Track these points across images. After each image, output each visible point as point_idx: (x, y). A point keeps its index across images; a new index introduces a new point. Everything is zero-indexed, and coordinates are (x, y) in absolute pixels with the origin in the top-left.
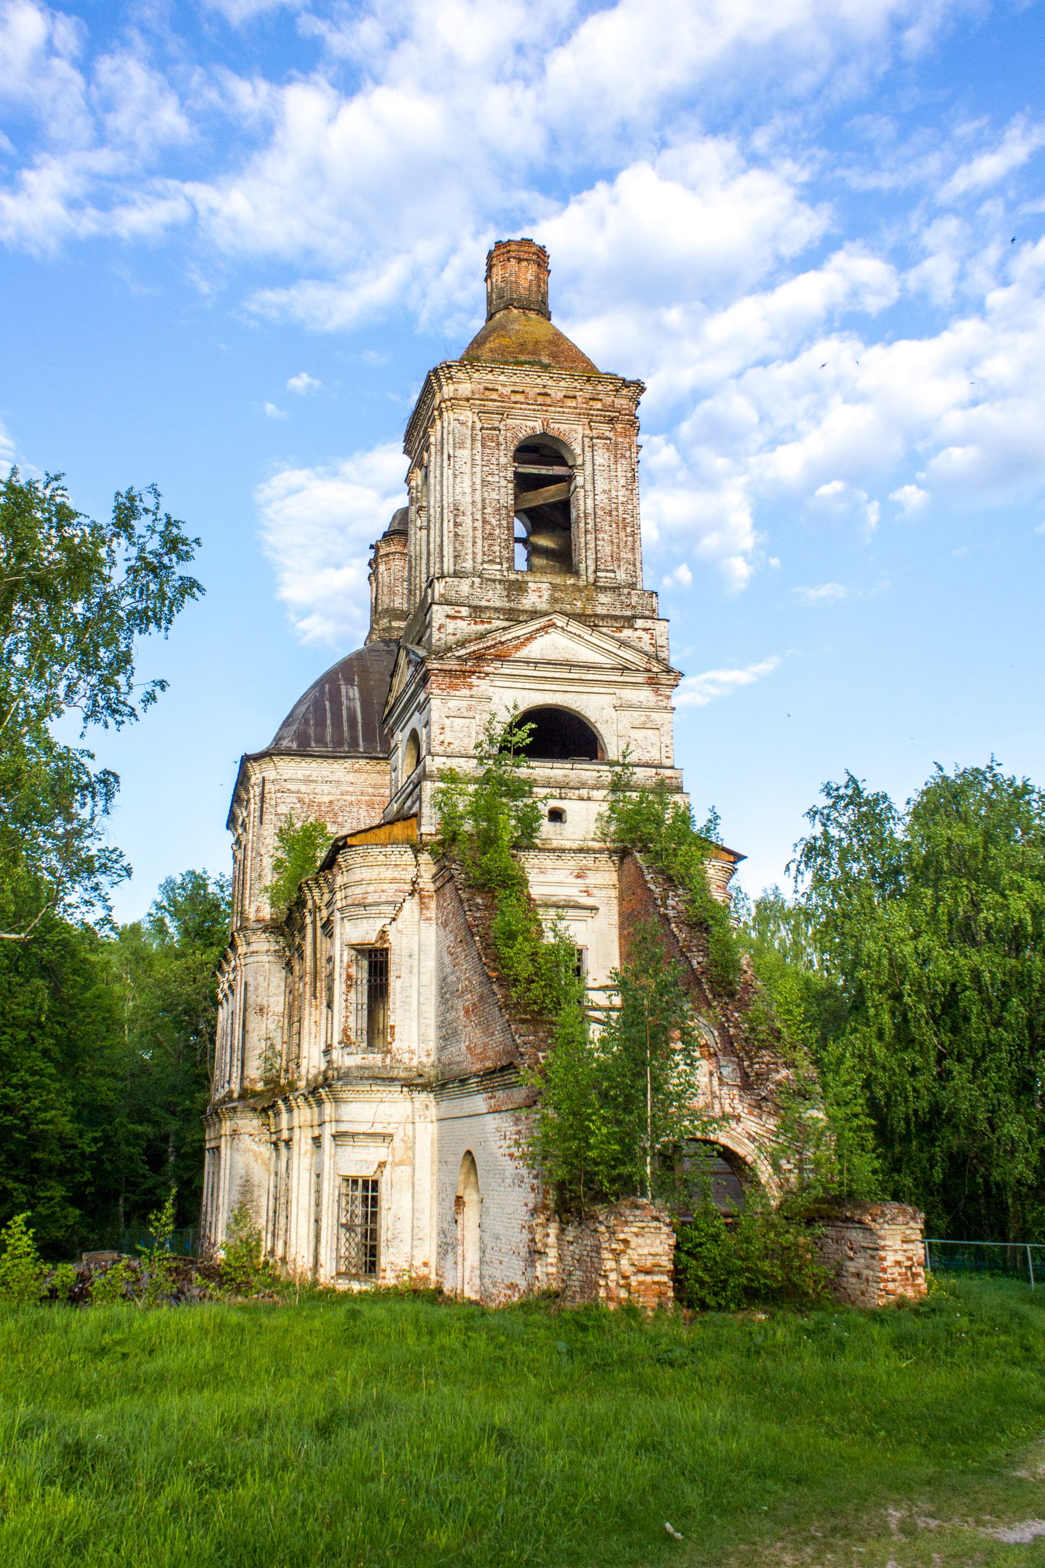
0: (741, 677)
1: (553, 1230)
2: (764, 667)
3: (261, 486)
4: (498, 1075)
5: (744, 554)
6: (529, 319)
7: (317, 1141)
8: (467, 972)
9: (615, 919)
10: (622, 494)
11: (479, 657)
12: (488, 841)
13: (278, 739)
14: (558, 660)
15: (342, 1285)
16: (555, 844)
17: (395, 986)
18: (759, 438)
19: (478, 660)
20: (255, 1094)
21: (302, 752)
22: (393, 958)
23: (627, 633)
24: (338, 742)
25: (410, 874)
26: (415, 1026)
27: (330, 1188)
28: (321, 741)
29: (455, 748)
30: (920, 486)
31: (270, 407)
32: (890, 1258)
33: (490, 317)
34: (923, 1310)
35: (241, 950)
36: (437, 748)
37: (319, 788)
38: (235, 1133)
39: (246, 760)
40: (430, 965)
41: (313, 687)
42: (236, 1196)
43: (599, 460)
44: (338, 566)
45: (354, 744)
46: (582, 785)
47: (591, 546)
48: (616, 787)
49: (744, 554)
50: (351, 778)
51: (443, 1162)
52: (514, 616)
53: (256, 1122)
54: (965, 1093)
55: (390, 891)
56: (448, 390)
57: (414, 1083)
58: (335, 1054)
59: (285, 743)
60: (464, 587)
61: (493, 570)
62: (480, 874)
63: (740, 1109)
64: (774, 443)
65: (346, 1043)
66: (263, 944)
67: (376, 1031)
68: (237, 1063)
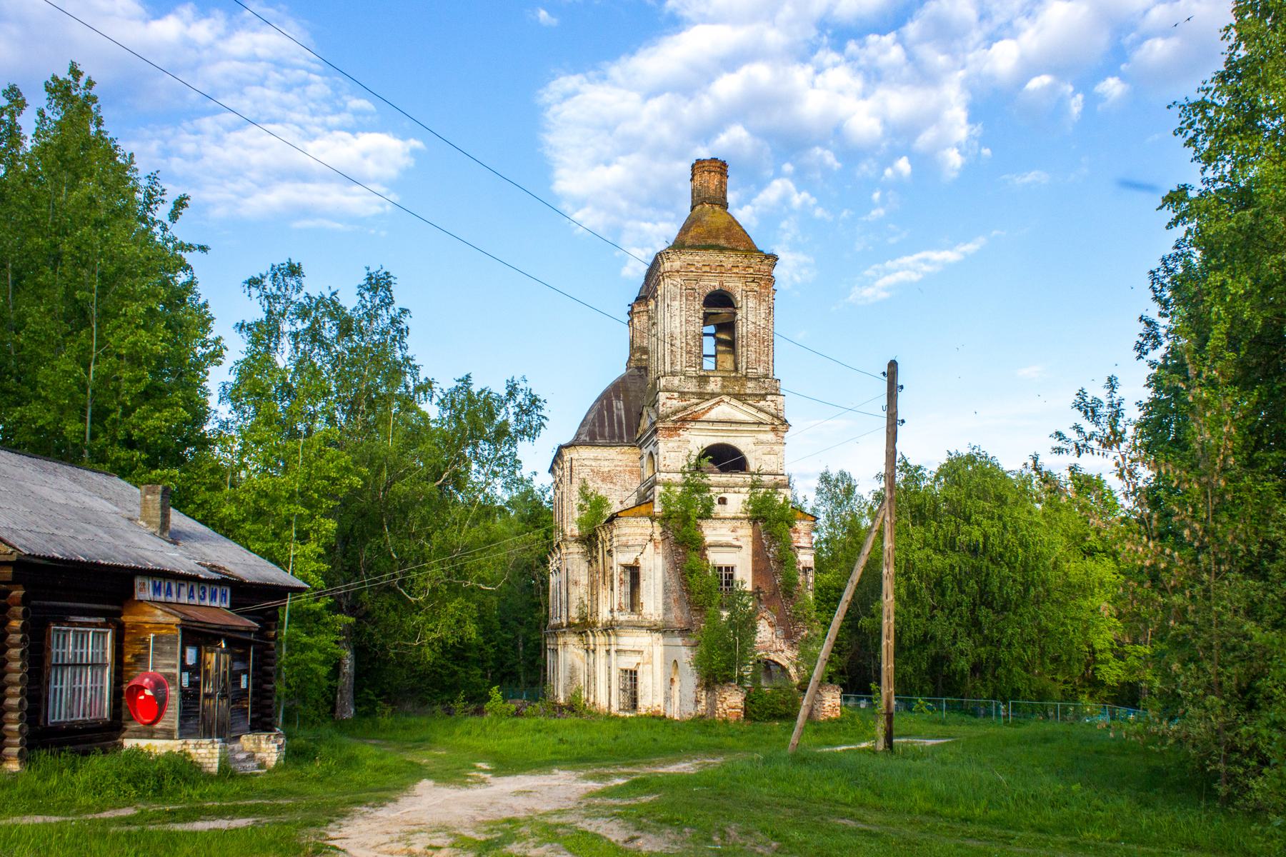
0: (950, 256)
1: (704, 693)
2: (970, 248)
3: (540, 92)
4: (684, 632)
5: (958, 146)
6: (714, 212)
7: (608, 652)
8: (674, 584)
9: (750, 552)
10: (762, 323)
11: (684, 420)
12: (686, 519)
13: (578, 435)
14: (726, 420)
15: (622, 714)
16: (721, 515)
17: (643, 584)
18: (977, 36)
19: (685, 420)
20: (575, 625)
21: (592, 443)
22: (642, 572)
23: (762, 403)
24: (612, 437)
25: (649, 531)
26: (653, 602)
27: (615, 674)
28: (602, 436)
29: (671, 468)
30: (1123, 78)
31: (543, 14)
32: (827, 704)
33: (693, 208)
34: (839, 721)
35: (564, 551)
36: (662, 468)
37: (603, 463)
38: (565, 644)
39: (561, 447)
40: (659, 575)
41: (597, 401)
42: (567, 674)
43: (750, 305)
44: (608, 164)
45: (621, 437)
46: (736, 485)
47: (747, 353)
48: (753, 486)
49: (958, 146)
50: (620, 457)
51: (666, 663)
52: (702, 396)
53: (576, 639)
54: (941, 627)
55: (640, 540)
56: (667, 265)
57: (653, 629)
58: (616, 614)
59: (583, 437)
60: (676, 381)
61: (691, 371)
62: (683, 536)
63: (784, 647)
64: (992, 39)
65: (620, 610)
66: (575, 548)
67: (634, 604)
68: (564, 610)
